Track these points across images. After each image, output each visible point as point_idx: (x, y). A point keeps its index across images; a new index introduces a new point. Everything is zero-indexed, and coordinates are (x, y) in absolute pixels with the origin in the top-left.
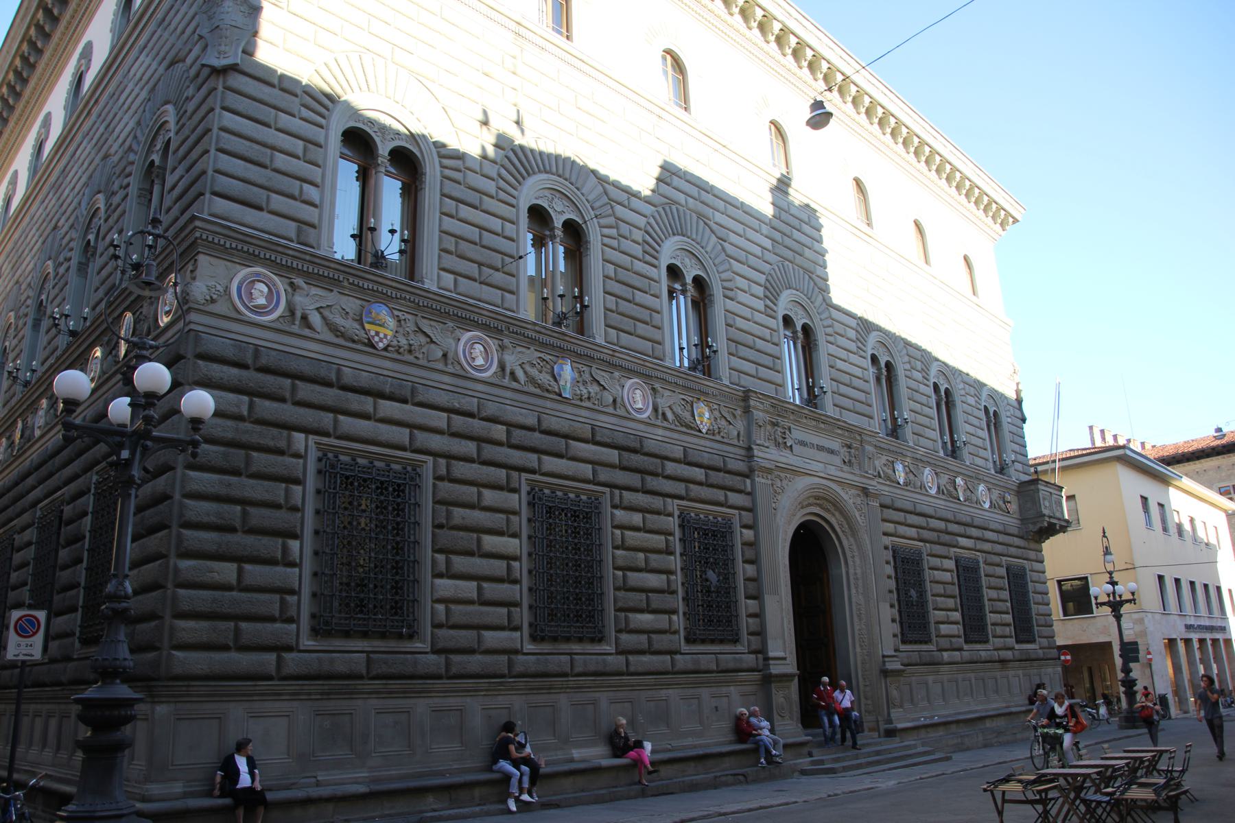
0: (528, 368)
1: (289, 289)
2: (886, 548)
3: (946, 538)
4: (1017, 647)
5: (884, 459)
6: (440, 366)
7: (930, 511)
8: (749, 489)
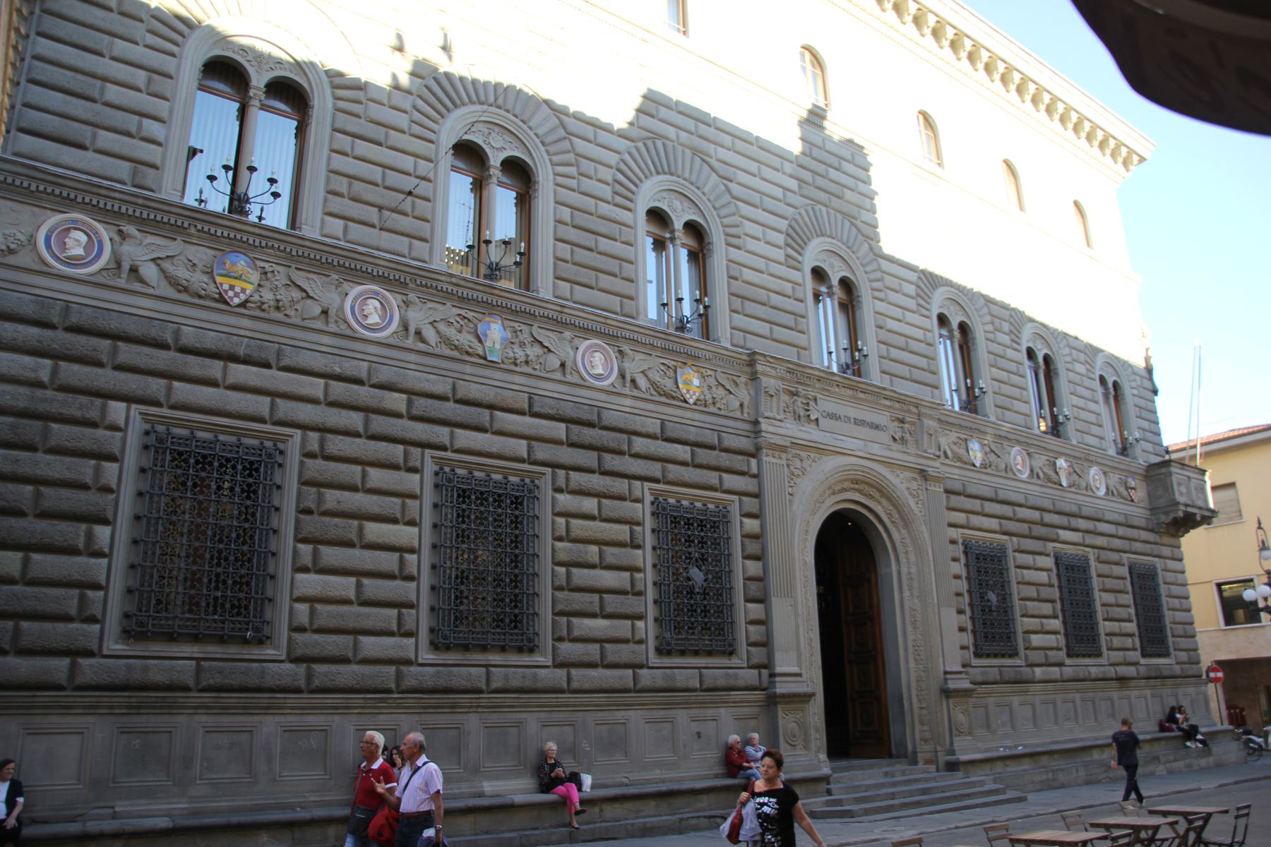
1: (117, 238)
2: (953, 542)
3: (1042, 531)
4: (1143, 661)
5: (953, 436)
6: (319, 324)
7: (1019, 498)
8: (754, 470)
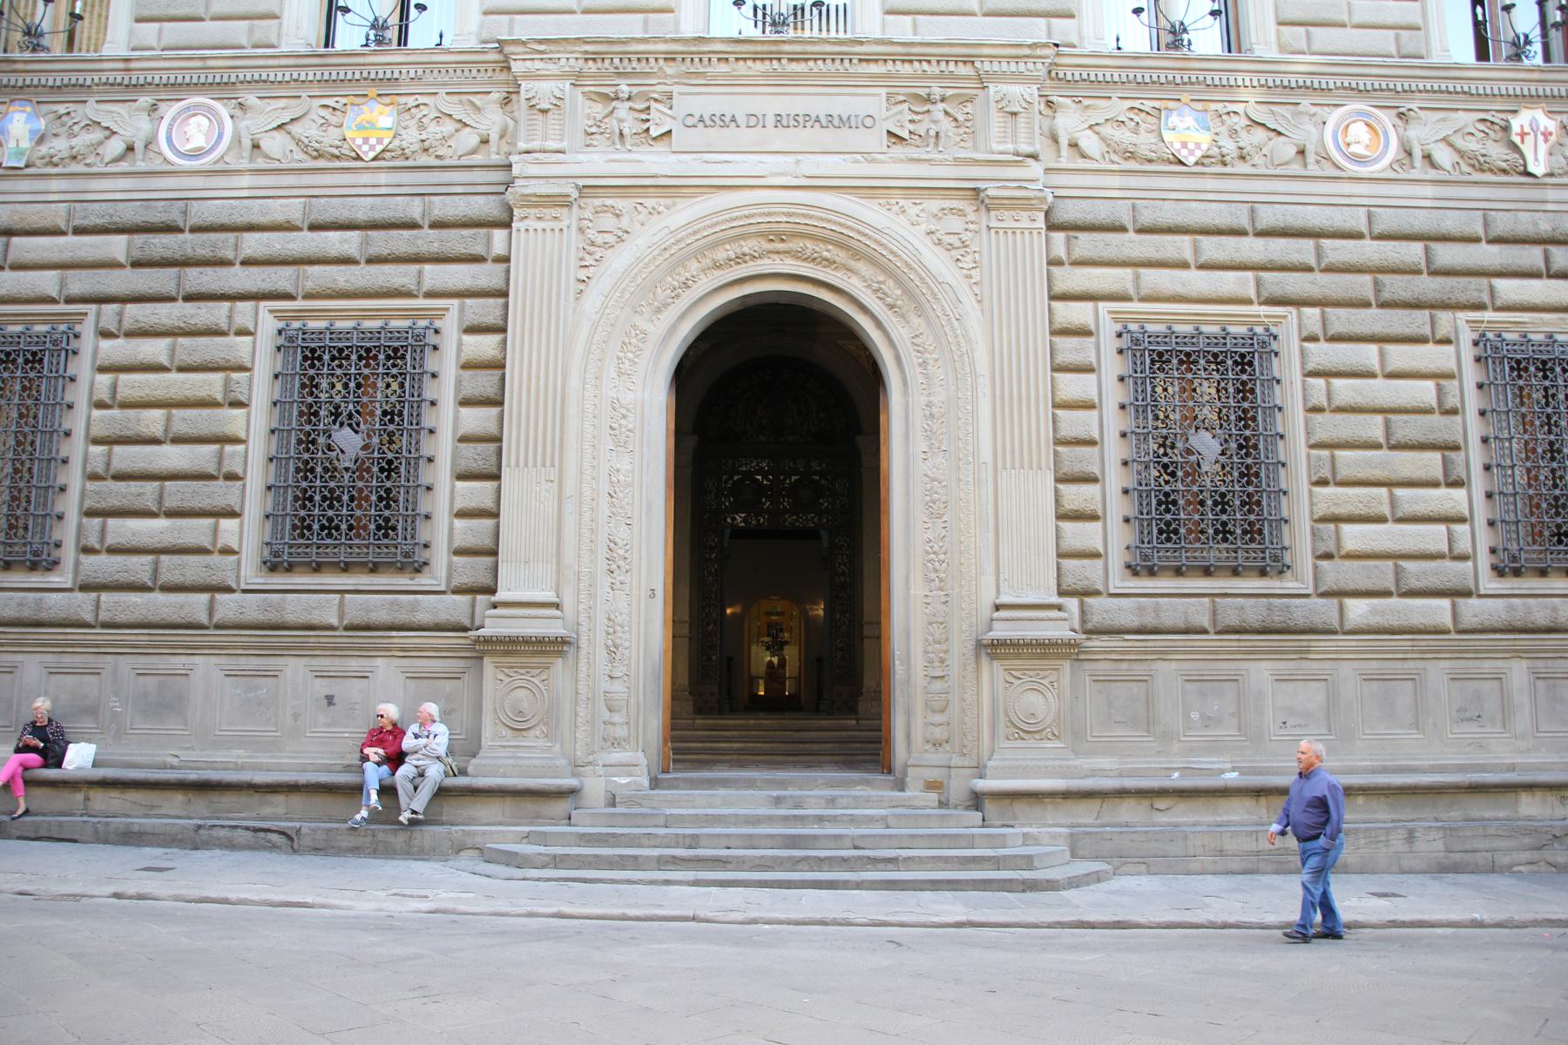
0: (1459, 142)
